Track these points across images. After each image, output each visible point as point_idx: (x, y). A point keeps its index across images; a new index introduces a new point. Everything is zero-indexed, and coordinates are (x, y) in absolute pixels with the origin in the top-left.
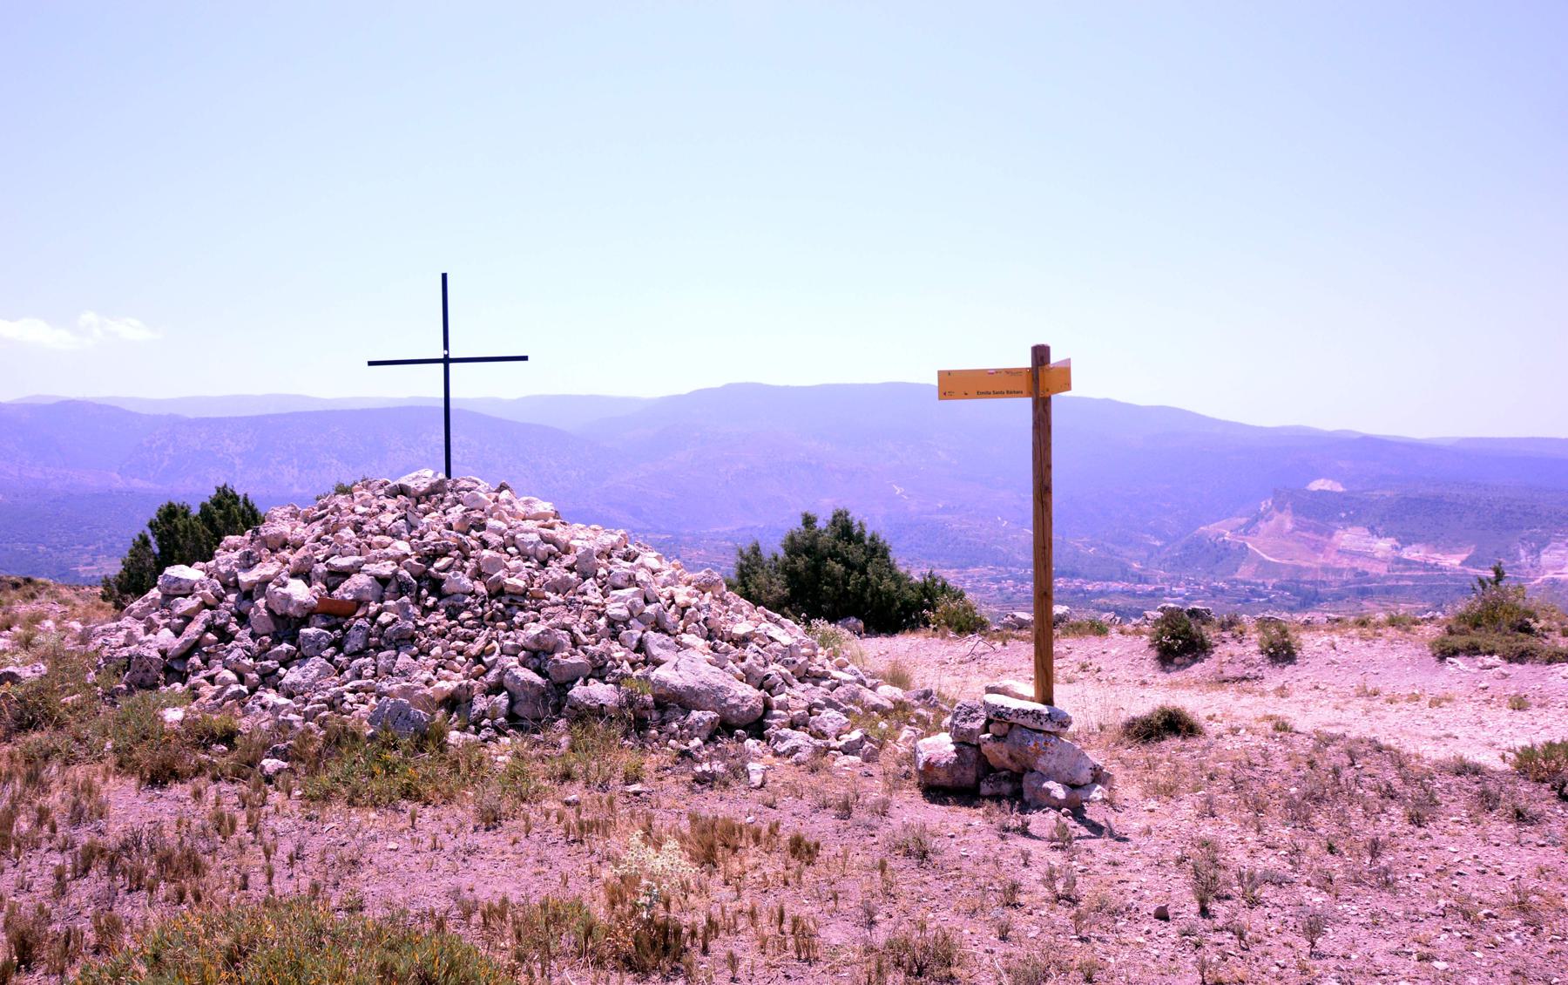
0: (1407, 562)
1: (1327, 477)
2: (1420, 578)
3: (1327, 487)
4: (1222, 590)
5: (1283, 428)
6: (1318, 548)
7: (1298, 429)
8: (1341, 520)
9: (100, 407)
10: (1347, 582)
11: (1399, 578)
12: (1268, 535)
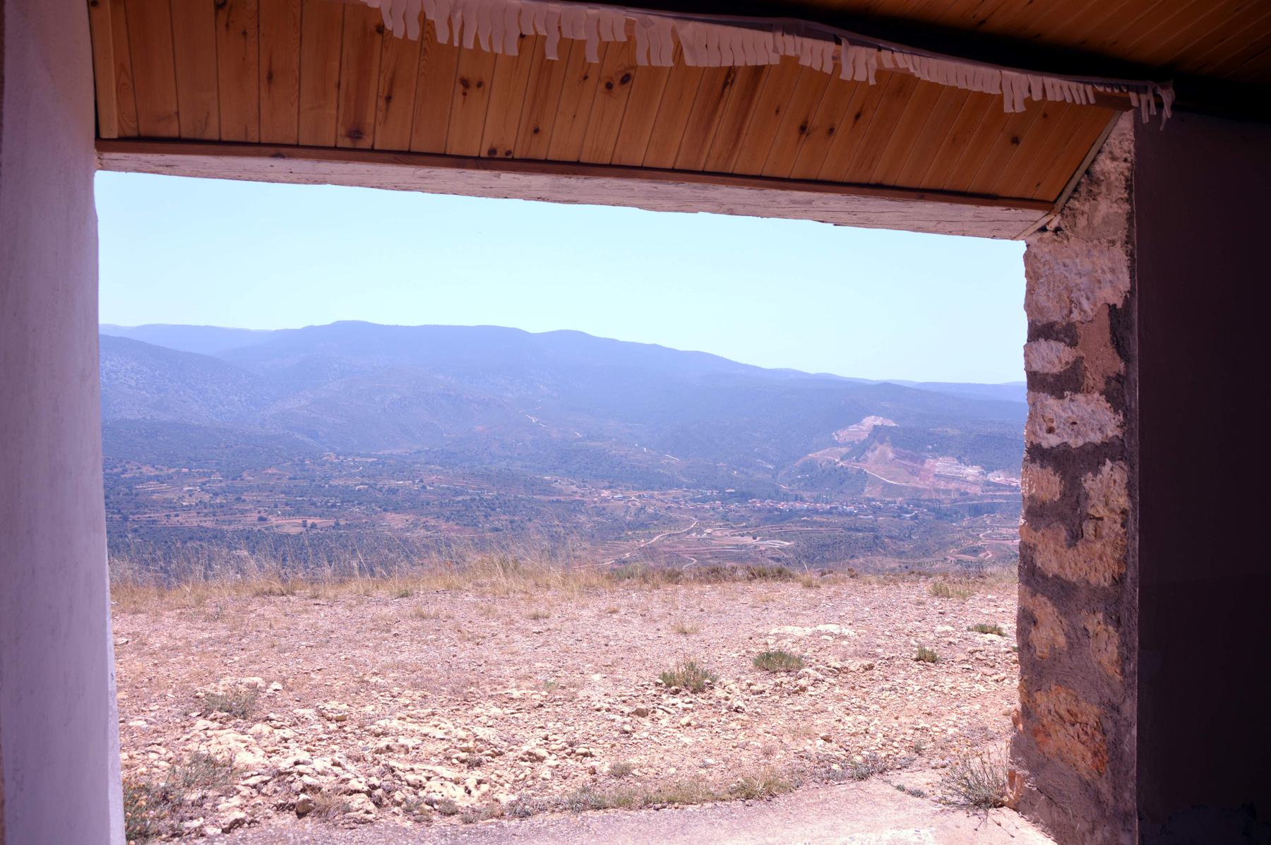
0: (995, 484)
2: (1007, 497)
4: (880, 508)
8: (929, 451)
9: (895, 386)
10: (955, 501)
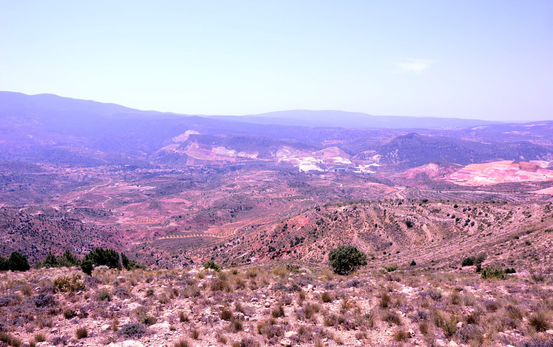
0: (241, 157)
3: (181, 136)
4: (193, 170)
5: (287, 111)
6: (207, 154)
8: (213, 145)
10: (225, 165)
11: (240, 163)
12: (191, 150)
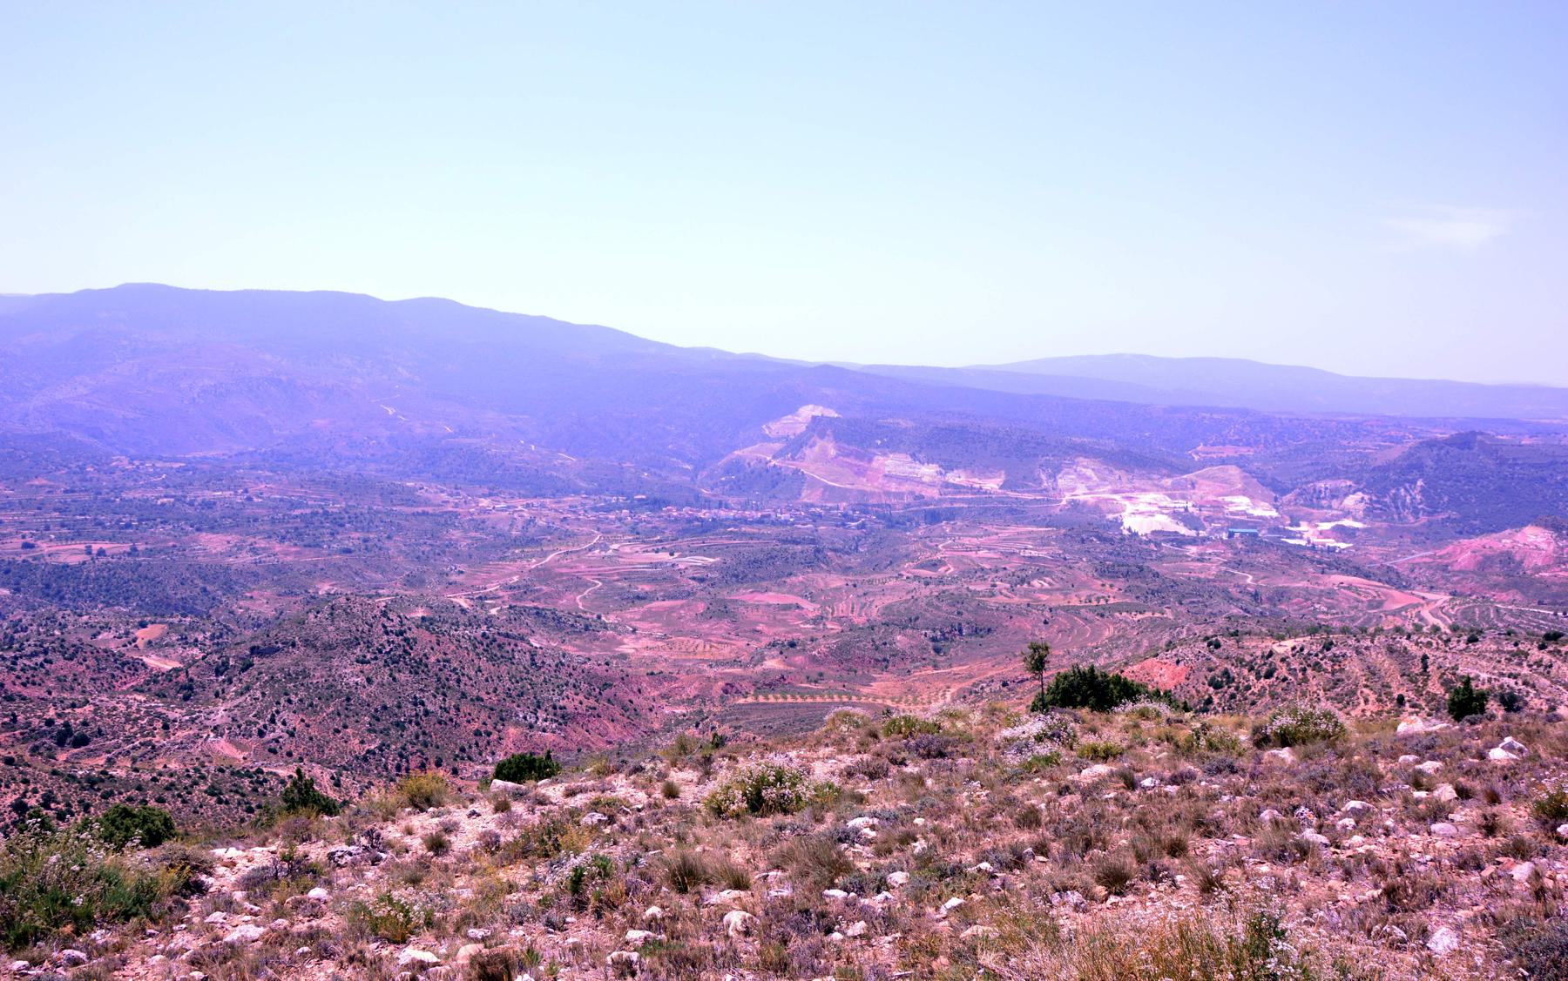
0: (955, 486)
1: (817, 403)
4: (820, 516)
5: (936, 370)
6: (860, 473)
7: (706, 352)
8: (878, 447)
10: (909, 505)
11: (953, 501)
